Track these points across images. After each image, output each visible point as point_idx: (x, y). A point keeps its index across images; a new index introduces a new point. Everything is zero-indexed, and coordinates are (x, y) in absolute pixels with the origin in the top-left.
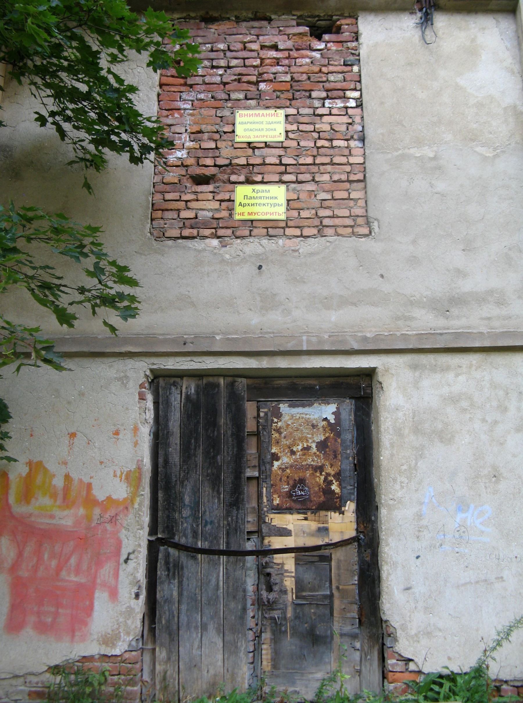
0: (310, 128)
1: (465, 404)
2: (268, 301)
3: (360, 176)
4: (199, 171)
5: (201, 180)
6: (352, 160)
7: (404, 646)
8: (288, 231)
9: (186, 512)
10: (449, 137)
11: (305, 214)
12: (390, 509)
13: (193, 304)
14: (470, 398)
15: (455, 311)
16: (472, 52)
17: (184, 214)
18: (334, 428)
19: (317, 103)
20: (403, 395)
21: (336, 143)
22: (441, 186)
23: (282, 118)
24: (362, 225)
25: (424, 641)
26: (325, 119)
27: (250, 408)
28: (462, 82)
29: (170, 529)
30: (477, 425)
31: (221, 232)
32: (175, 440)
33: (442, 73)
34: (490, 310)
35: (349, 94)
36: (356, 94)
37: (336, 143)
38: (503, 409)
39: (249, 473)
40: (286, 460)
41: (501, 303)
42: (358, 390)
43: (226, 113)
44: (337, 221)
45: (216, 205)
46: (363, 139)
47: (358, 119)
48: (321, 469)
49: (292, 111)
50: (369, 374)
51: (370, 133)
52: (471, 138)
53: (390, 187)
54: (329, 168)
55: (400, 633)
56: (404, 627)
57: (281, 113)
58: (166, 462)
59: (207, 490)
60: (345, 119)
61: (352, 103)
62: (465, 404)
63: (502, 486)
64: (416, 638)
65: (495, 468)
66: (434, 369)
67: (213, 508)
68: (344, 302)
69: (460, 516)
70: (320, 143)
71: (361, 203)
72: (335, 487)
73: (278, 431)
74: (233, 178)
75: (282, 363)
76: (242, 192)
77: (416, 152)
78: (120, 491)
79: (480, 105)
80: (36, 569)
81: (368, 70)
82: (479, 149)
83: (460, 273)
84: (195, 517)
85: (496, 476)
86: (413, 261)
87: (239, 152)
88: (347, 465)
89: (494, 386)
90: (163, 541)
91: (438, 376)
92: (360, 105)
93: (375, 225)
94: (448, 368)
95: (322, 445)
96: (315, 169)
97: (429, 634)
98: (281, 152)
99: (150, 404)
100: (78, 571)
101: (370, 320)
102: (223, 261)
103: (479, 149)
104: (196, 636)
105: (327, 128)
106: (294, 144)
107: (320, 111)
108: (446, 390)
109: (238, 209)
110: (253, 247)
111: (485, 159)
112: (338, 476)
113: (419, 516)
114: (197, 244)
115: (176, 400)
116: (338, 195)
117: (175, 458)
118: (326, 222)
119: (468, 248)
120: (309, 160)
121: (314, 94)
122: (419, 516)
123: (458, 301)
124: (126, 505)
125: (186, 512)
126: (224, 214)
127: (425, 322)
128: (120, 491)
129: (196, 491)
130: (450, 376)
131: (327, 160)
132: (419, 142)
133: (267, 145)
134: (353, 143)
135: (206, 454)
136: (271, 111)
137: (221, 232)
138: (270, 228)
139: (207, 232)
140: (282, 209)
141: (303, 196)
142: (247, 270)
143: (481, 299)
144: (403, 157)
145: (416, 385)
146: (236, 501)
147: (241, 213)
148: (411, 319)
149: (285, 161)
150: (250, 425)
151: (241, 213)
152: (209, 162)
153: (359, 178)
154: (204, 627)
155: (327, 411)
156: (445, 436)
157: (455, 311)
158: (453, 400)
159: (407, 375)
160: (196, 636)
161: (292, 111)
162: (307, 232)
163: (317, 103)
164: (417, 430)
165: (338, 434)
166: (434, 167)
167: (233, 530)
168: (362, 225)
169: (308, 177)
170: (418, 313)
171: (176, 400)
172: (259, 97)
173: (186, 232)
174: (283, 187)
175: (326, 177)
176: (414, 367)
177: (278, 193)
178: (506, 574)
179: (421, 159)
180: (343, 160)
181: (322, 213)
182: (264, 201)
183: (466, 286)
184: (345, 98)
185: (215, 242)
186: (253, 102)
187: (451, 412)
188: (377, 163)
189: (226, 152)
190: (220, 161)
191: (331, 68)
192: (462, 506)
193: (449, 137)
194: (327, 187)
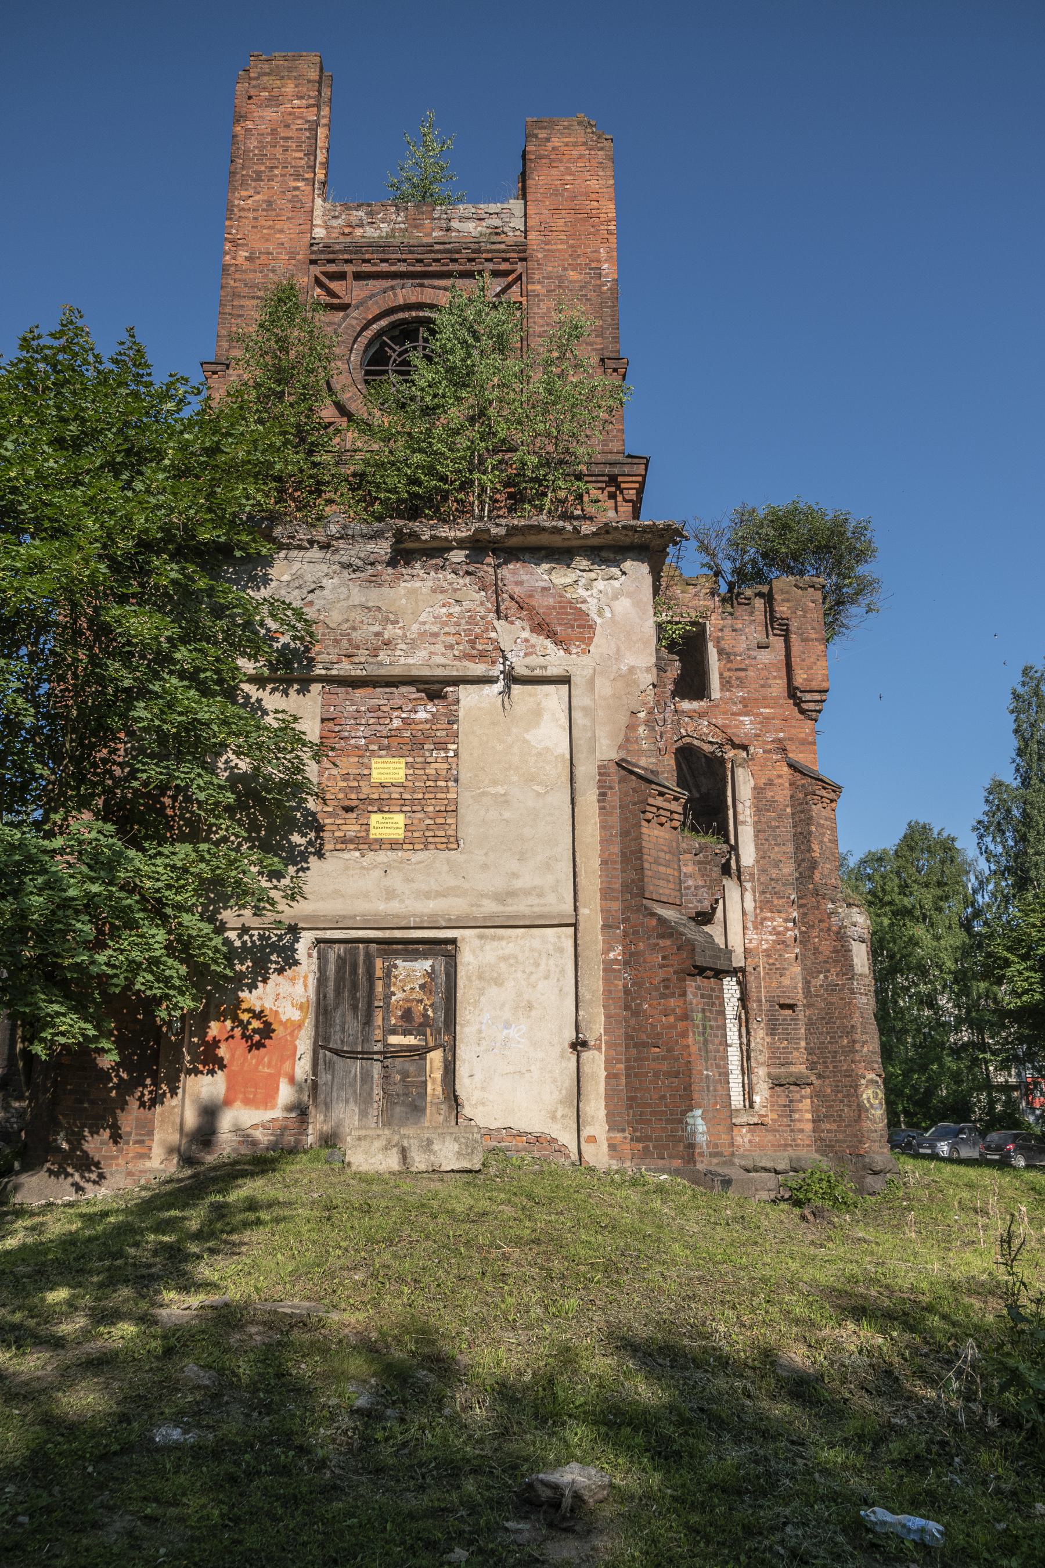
0: (422, 772)
1: (512, 961)
2: (390, 894)
3: (453, 808)
4: (347, 803)
5: (348, 809)
6: (449, 796)
7: (467, 1111)
8: (405, 846)
9: (338, 1028)
10: (515, 778)
11: (416, 834)
12: (462, 1026)
13: (342, 896)
14: (516, 957)
15: (509, 901)
16: (537, 714)
17: (337, 834)
18: (431, 975)
19: (427, 754)
20: (474, 954)
21: (439, 783)
22: (507, 815)
23: (403, 765)
24: (452, 842)
25: (480, 1108)
26: (433, 765)
27: (379, 963)
28: (528, 737)
29: (327, 1039)
30: (519, 975)
31: (361, 847)
32: (331, 984)
33: (514, 730)
34: (533, 900)
35: (450, 746)
36: (454, 747)
37: (439, 783)
38: (537, 965)
39: (377, 1004)
40: (400, 995)
41: (540, 895)
42: (445, 950)
43: (366, 760)
44: (437, 840)
45: (358, 828)
46: (456, 781)
47: (454, 766)
48: (421, 1001)
49: (410, 760)
50: (453, 941)
51: (461, 777)
52: (531, 779)
53: (474, 818)
54: (433, 802)
55: (465, 1103)
56: (468, 1099)
57: (403, 760)
58: (325, 997)
59: (349, 1017)
60: (446, 766)
61: (451, 754)
62: (512, 961)
63: (533, 1013)
64: (475, 1106)
65: (529, 1002)
66: (494, 938)
67: (354, 1026)
68: (439, 895)
69: (506, 1032)
70: (428, 783)
71: (453, 827)
72: (430, 1013)
73: (396, 977)
74: (370, 808)
75: (731, 812)
76: (375, 819)
77: (492, 790)
78: (296, 1015)
79: (539, 754)
80: (243, 1065)
81: (463, 727)
82: (535, 787)
83: (515, 875)
84: (343, 1030)
85: (530, 1007)
86: (485, 867)
87: (374, 790)
88: (438, 998)
89: (532, 950)
90: (321, 1043)
91: (496, 943)
92: (456, 755)
93: (461, 842)
94: (501, 938)
95: (422, 987)
96: (423, 802)
97: (483, 1104)
98: (401, 790)
99: (315, 960)
100: (269, 1066)
101: (455, 906)
102: (363, 868)
103: (535, 787)
104: (342, 1105)
105: (433, 772)
106: (410, 784)
107: (429, 760)
108: (500, 952)
109: (372, 831)
110: (383, 857)
111: (538, 794)
112: (432, 1005)
113: (480, 1031)
114: (346, 855)
115: (332, 957)
116: (438, 821)
117: (331, 994)
118: (430, 840)
119: (522, 858)
120: (420, 796)
121: (426, 747)
122: (480, 1031)
123: (512, 894)
124: (300, 1026)
125: (338, 1028)
126: (363, 834)
127: (490, 907)
128: (296, 1015)
129: (344, 1015)
130: (504, 943)
131: (432, 796)
132: (495, 783)
133: (393, 785)
134: (450, 784)
135: (350, 991)
136: (396, 760)
137: (361, 847)
138: (394, 845)
139: (352, 847)
140: (401, 831)
141: (415, 822)
142: (378, 873)
143: (527, 892)
144: (483, 794)
145: (482, 949)
146: (368, 1021)
147: (374, 834)
148: (480, 906)
149: (405, 796)
150: (379, 973)
151: (374, 834)
152: (353, 796)
153: (452, 809)
154: (347, 1101)
155: (426, 964)
156: (498, 982)
157: (509, 901)
158: (505, 958)
159: (477, 942)
160: (342, 1105)
161: (410, 760)
162: (417, 847)
163: (427, 754)
164: (480, 978)
165: (433, 980)
166: (504, 801)
167: (366, 1040)
168: (452, 842)
169: (419, 808)
170: (485, 902)
171: (332, 957)
172: (388, 748)
173: (338, 847)
174: (402, 816)
175: (431, 809)
176: (481, 937)
177: (400, 819)
178: (532, 1068)
179: (495, 795)
180: (443, 796)
181: (428, 833)
182: (388, 825)
183: (518, 884)
184: (447, 750)
185: (357, 854)
186: (383, 753)
187: (503, 966)
188: (466, 799)
189: (365, 790)
190: (361, 796)
191: (439, 726)
192: (507, 1025)
193: (515, 778)
194: (431, 815)
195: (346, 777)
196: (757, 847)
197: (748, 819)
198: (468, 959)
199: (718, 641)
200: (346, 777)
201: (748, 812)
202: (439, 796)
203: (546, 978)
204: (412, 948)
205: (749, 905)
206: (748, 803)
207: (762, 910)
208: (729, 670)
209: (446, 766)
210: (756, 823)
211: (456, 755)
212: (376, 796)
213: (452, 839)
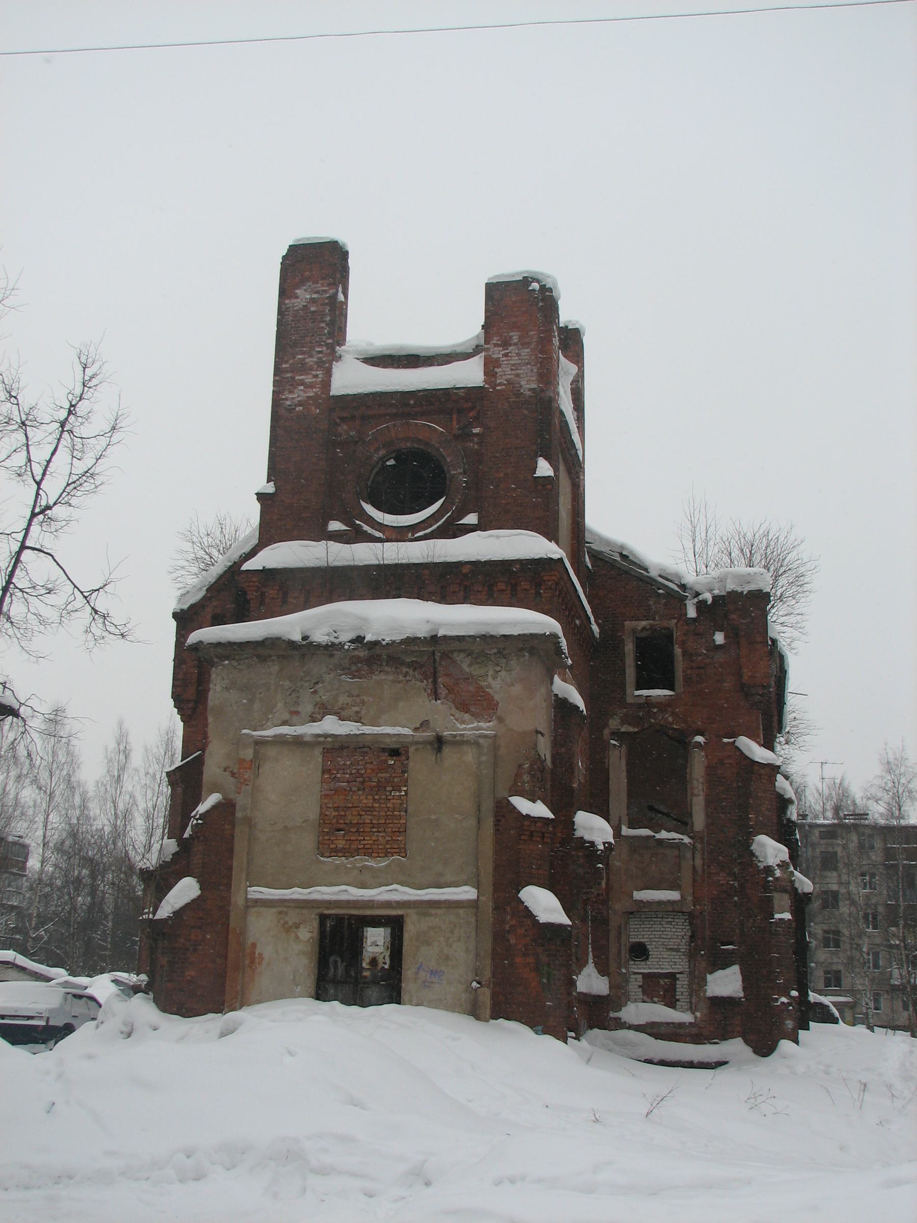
11: (380, 847)
17: (332, 846)
30: (442, 939)
36: (405, 788)
38: (452, 932)
43: (349, 798)
46: (406, 811)
51: (410, 809)
60: (399, 801)
61: (403, 793)
121: (388, 789)
139: (341, 854)
142: (356, 872)
152: (342, 821)
153: (403, 831)
168: (402, 851)
190: (347, 822)
195: (337, 808)
196: (708, 816)
197: (701, 793)
198: (410, 929)
199: (683, 644)
200: (337, 808)
201: (701, 787)
202: (395, 821)
203: (459, 940)
204: (376, 922)
205: (698, 862)
206: (701, 780)
207: (709, 867)
208: (692, 668)
209: (399, 801)
210: (707, 795)
211: (406, 794)
212: (356, 821)
213: (402, 850)
